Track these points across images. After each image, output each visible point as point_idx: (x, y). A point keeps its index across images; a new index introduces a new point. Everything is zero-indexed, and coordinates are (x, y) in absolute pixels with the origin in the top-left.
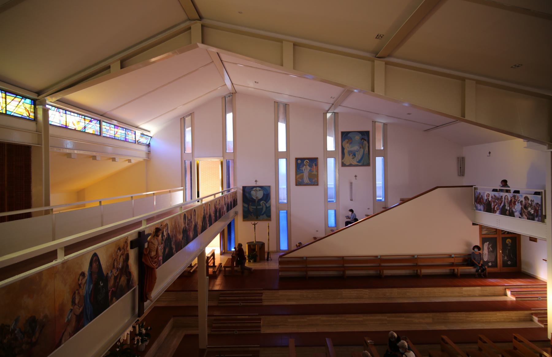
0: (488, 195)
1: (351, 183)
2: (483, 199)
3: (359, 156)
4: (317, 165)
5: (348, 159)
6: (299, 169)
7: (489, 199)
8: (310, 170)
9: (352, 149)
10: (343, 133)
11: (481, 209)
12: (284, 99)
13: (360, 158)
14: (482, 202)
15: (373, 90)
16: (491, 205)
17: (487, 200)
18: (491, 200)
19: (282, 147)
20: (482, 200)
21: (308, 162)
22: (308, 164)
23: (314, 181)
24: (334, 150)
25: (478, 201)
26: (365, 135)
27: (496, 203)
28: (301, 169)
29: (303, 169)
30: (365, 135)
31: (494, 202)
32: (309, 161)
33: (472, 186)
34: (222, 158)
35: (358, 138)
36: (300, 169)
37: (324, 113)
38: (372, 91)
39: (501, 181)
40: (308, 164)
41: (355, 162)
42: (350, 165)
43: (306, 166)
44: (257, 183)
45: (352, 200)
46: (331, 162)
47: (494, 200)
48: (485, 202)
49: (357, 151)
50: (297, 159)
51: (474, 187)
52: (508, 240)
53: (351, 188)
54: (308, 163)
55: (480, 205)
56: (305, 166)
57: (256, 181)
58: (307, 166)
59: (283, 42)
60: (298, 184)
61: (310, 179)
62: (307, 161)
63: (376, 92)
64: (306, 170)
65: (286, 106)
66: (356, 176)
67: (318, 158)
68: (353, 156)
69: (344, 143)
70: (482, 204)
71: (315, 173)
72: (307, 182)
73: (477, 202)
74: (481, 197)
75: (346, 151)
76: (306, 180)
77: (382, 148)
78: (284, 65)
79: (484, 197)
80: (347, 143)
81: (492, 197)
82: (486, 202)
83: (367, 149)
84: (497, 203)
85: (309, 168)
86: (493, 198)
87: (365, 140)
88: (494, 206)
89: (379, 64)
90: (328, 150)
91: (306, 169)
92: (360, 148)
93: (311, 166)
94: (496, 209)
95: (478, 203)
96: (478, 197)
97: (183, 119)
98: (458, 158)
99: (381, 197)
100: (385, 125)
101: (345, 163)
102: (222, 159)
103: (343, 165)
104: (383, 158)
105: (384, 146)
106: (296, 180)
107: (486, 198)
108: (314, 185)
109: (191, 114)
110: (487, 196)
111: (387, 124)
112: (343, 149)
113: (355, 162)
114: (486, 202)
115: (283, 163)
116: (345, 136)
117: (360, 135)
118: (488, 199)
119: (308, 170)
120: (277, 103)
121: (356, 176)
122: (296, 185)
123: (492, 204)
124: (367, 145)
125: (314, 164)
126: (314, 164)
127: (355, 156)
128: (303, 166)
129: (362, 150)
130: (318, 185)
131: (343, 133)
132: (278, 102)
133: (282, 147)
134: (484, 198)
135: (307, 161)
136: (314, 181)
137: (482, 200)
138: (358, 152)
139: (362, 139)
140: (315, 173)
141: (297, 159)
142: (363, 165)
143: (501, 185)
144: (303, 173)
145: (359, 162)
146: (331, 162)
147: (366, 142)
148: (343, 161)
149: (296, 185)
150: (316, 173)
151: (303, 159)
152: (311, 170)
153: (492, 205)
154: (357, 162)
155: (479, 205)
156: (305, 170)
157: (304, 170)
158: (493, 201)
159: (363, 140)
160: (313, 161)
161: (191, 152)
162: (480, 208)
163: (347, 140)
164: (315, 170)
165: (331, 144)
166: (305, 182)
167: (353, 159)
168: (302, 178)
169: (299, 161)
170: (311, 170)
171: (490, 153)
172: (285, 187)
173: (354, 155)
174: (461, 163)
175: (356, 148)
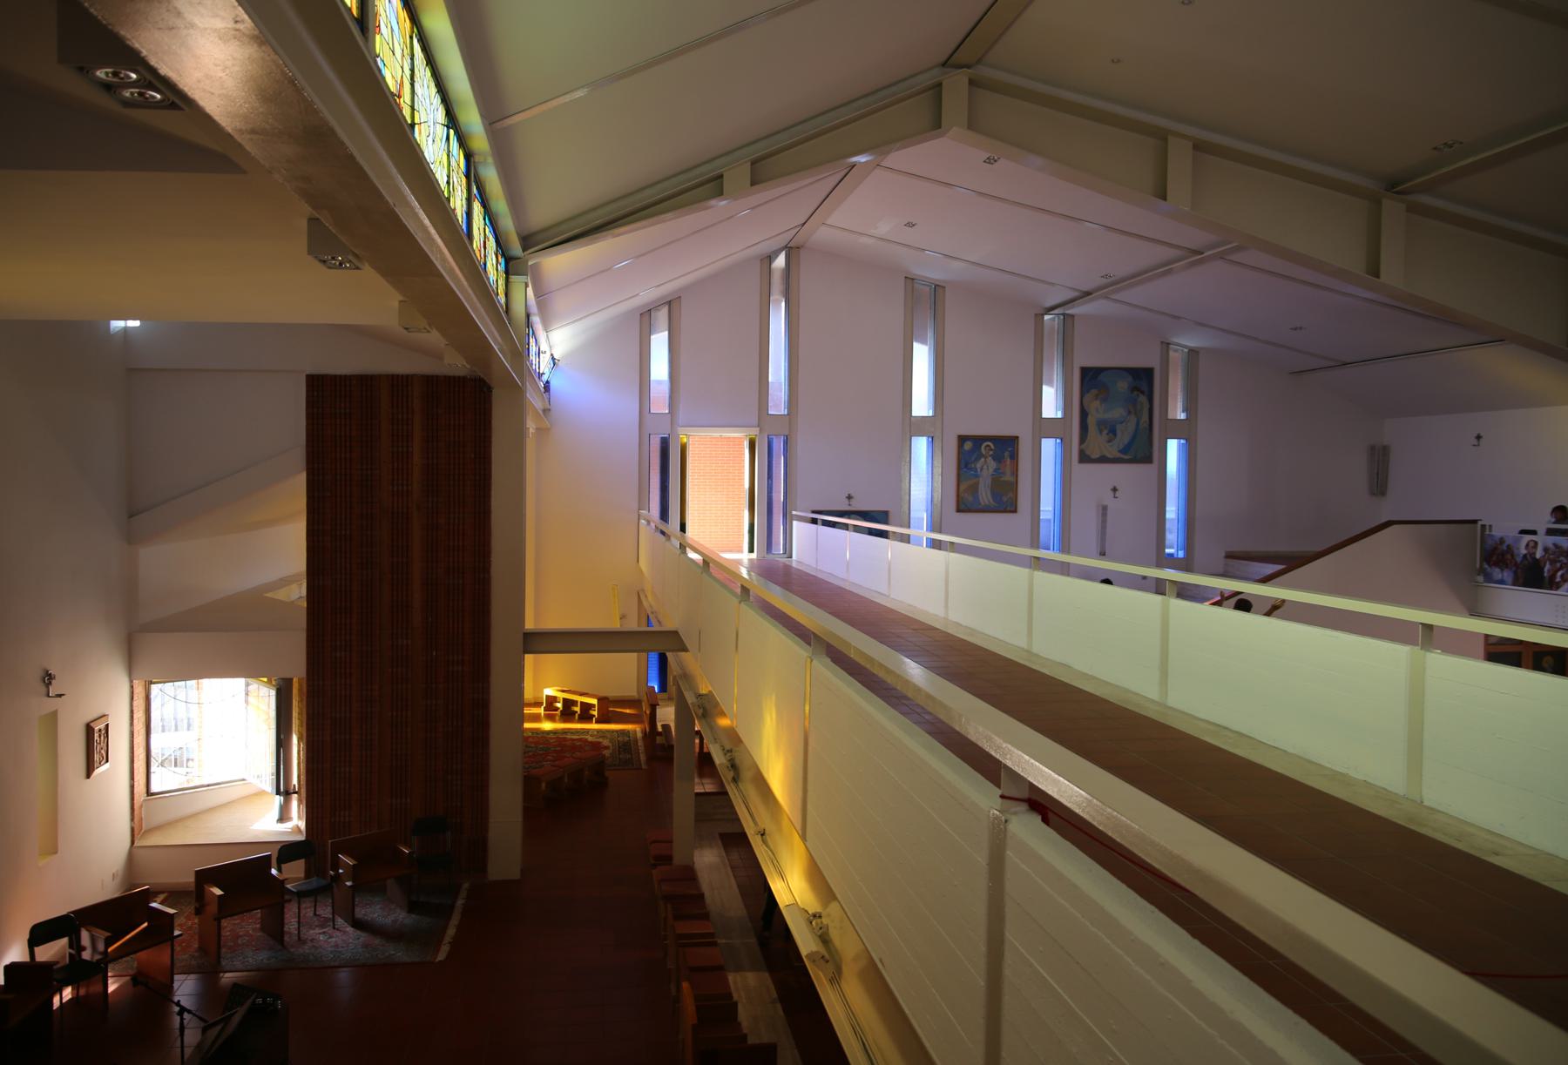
0: (1532, 544)
1: (1105, 508)
2: (1512, 555)
3: (1123, 437)
4: (1014, 456)
5: (1098, 442)
6: (966, 466)
7: (1534, 554)
8: (995, 470)
9: (1108, 416)
10: (1085, 371)
11: (1505, 578)
12: (933, 271)
13: (1126, 440)
14: (1508, 562)
15: (1375, 272)
16: (1543, 569)
17: (1528, 556)
18: (1544, 556)
19: (922, 404)
20: (1509, 556)
21: (992, 447)
22: (991, 453)
23: (1005, 499)
24: (931, 414)
25: (1494, 558)
26: (1142, 380)
27: (1558, 565)
28: (973, 466)
29: (979, 465)
30: (1142, 380)
31: (1553, 562)
32: (993, 443)
33: (1475, 522)
34: (758, 429)
35: (1123, 385)
36: (969, 466)
37: (1036, 314)
38: (1368, 273)
39: (1550, 510)
40: (991, 453)
41: (1112, 450)
42: (1103, 460)
43: (986, 458)
44: (853, 502)
45: (1104, 555)
46: (1049, 447)
47: (1551, 557)
48: (1522, 561)
49: (1122, 423)
50: (962, 439)
51: (1480, 523)
52: (1546, 659)
53: (1104, 522)
54: (992, 450)
55: (1502, 570)
56: (983, 460)
57: (849, 497)
58: (990, 459)
59: (1170, 138)
60: (962, 507)
61: (995, 495)
62: (988, 446)
63: (1384, 278)
64: (987, 467)
65: (938, 288)
66: (1115, 490)
67: (1017, 437)
68: (1111, 435)
69: (1088, 397)
70: (1507, 567)
71: (1008, 477)
72: (987, 503)
73: (1492, 563)
74: (1505, 548)
75: (1091, 421)
76: (985, 496)
77: (1182, 416)
78: (1168, 197)
79: (1518, 549)
80: (1096, 399)
81: (1546, 550)
82: (1526, 562)
83: (1145, 417)
84: (1565, 564)
85: (992, 464)
86: (1550, 552)
87: (1142, 392)
88: (1551, 573)
89: (1392, 209)
90: (1044, 416)
91: (985, 467)
92: (1130, 412)
93: (998, 458)
94: (1558, 579)
95: (1496, 564)
96: (1496, 548)
97: (645, 319)
98: (1373, 448)
99: (1173, 548)
100: (1193, 353)
101: (1088, 453)
102: (754, 432)
103: (1084, 458)
104: (1058, 441)
105: (1186, 410)
106: (958, 496)
107: (1524, 551)
108: (1005, 511)
109: (671, 303)
110: (1527, 545)
111: (1198, 352)
112: (1084, 414)
113: (1112, 450)
114: (1526, 562)
115: (920, 446)
116: (1091, 381)
117: (1130, 379)
118: (1530, 555)
119: (991, 470)
120: (910, 280)
121: (1115, 490)
122: (958, 510)
123: (1547, 567)
124: (1146, 406)
125: (1007, 454)
126: (1007, 454)
127: (1115, 434)
128: (977, 459)
129: (1133, 420)
130: (1015, 511)
131: (1085, 371)
132: (913, 279)
133: (922, 404)
134: (1516, 552)
135: (989, 443)
136: (1005, 499)
137: (1509, 556)
138: (1124, 424)
139: (1134, 389)
140: (1008, 477)
141: (962, 439)
142: (1134, 460)
143: (1553, 520)
144: (977, 476)
145: (1123, 451)
146: (1049, 447)
147: (1143, 399)
148: (1083, 446)
149: (958, 510)
150: (1012, 479)
151: (978, 440)
152: (999, 469)
153: (1546, 569)
154: (1120, 451)
155: (1497, 570)
156: (981, 470)
157: (979, 470)
158: (1549, 560)
159: (1136, 393)
160: (1006, 447)
161: (783, 411)
162: (1503, 576)
163: (1094, 392)
164: (1008, 471)
165: (1051, 404)
166: (983, 504)
167: (1110, 444)
168: (974, 489)
169: (968, 445)
170: (999, 469)
171: (1479, 437)
172: (1051, 509)
173: (1113, 432)
174: (1379, 461)
175: (1117, 413)
